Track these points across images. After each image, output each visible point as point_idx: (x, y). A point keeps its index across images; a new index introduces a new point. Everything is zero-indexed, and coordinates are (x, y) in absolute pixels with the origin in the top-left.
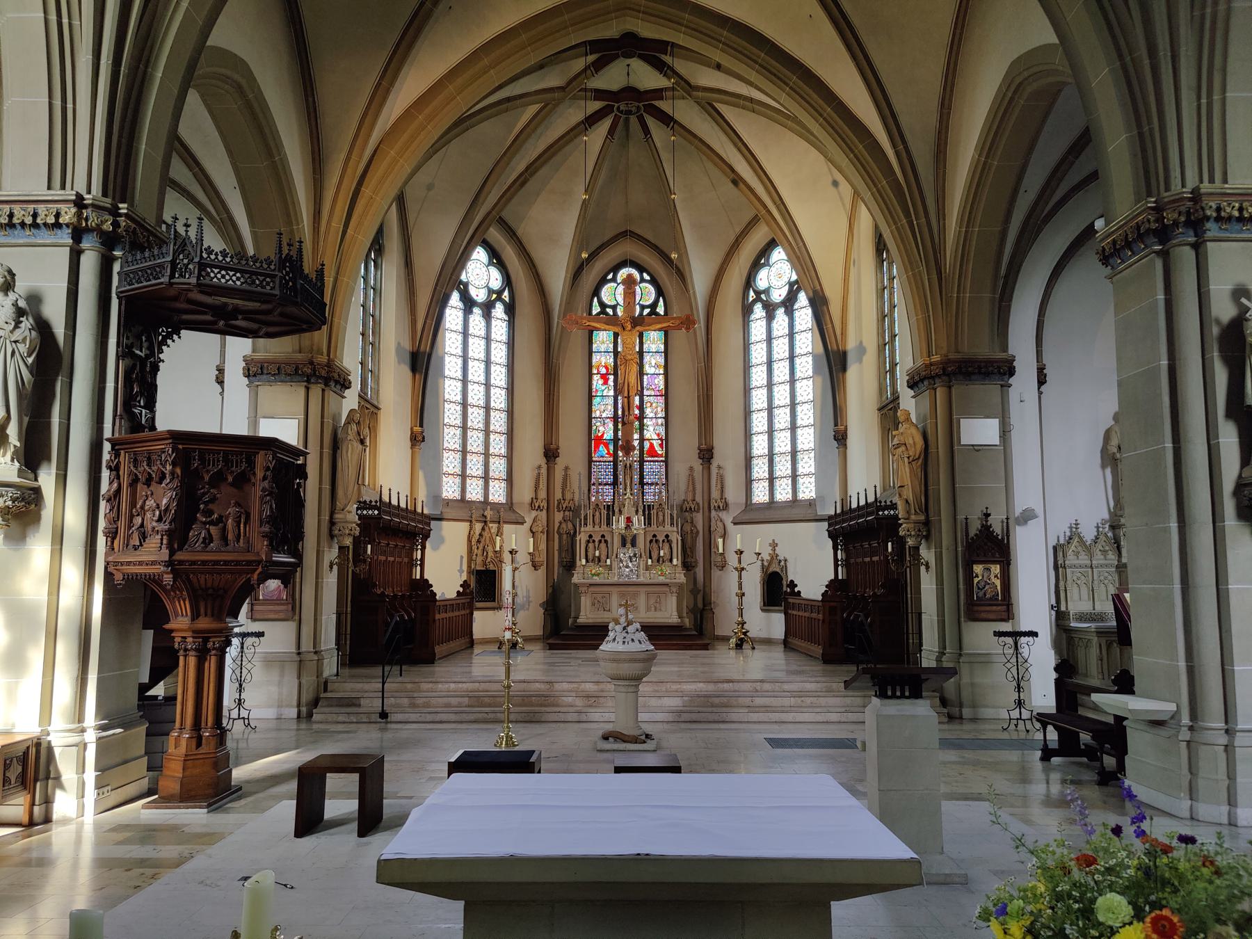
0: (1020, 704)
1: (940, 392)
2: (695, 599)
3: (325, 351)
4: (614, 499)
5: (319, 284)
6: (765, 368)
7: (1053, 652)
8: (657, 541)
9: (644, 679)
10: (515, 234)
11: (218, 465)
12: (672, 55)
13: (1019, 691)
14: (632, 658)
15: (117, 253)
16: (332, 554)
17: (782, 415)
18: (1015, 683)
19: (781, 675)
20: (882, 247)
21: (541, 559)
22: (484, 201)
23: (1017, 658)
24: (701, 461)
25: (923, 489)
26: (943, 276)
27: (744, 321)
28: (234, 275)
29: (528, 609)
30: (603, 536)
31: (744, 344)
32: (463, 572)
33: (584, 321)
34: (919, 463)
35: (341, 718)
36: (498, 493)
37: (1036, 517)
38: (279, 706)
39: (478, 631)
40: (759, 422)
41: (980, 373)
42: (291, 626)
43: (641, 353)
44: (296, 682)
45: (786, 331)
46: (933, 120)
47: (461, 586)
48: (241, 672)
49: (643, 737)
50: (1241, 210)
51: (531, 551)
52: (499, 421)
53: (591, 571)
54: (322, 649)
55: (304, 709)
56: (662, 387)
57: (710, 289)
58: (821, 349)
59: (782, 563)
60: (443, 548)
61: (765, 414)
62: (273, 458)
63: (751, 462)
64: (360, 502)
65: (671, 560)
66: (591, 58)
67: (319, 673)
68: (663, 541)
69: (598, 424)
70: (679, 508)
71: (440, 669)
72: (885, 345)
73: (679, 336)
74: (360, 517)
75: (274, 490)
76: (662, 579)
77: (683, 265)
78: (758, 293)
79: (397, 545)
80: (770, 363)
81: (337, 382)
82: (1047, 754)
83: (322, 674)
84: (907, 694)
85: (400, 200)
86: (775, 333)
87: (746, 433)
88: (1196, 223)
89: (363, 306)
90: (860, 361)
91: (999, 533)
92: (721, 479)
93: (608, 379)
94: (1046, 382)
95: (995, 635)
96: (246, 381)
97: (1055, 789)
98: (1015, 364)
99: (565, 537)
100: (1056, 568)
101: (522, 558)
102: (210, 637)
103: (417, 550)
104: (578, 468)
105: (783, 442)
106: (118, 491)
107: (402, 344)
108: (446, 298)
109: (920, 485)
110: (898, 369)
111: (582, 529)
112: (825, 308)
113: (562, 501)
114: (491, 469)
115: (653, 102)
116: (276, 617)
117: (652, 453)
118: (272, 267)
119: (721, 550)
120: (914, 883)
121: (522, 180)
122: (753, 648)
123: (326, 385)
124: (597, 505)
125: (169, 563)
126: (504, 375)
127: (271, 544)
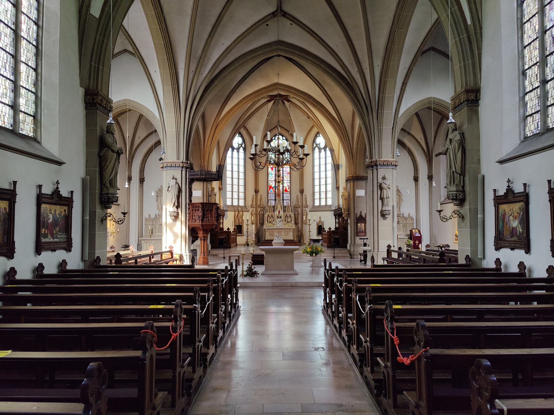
2: (298, 233)
30: (272, 215)
36: (242, 203)
40: (317, 182)
46: (351, 118)
50: (384, 163)
60: (227, 219)
65: (291, 222)
71: (232, 249)
76: (288, 227)
78: (316, 145)
88: (377, 166)
92: (306, 198)
101: (250, 222)
104: (265, 195)
105: (323, 188)
106: (190, 212)
117: (286, 190)
125: (202, 225)
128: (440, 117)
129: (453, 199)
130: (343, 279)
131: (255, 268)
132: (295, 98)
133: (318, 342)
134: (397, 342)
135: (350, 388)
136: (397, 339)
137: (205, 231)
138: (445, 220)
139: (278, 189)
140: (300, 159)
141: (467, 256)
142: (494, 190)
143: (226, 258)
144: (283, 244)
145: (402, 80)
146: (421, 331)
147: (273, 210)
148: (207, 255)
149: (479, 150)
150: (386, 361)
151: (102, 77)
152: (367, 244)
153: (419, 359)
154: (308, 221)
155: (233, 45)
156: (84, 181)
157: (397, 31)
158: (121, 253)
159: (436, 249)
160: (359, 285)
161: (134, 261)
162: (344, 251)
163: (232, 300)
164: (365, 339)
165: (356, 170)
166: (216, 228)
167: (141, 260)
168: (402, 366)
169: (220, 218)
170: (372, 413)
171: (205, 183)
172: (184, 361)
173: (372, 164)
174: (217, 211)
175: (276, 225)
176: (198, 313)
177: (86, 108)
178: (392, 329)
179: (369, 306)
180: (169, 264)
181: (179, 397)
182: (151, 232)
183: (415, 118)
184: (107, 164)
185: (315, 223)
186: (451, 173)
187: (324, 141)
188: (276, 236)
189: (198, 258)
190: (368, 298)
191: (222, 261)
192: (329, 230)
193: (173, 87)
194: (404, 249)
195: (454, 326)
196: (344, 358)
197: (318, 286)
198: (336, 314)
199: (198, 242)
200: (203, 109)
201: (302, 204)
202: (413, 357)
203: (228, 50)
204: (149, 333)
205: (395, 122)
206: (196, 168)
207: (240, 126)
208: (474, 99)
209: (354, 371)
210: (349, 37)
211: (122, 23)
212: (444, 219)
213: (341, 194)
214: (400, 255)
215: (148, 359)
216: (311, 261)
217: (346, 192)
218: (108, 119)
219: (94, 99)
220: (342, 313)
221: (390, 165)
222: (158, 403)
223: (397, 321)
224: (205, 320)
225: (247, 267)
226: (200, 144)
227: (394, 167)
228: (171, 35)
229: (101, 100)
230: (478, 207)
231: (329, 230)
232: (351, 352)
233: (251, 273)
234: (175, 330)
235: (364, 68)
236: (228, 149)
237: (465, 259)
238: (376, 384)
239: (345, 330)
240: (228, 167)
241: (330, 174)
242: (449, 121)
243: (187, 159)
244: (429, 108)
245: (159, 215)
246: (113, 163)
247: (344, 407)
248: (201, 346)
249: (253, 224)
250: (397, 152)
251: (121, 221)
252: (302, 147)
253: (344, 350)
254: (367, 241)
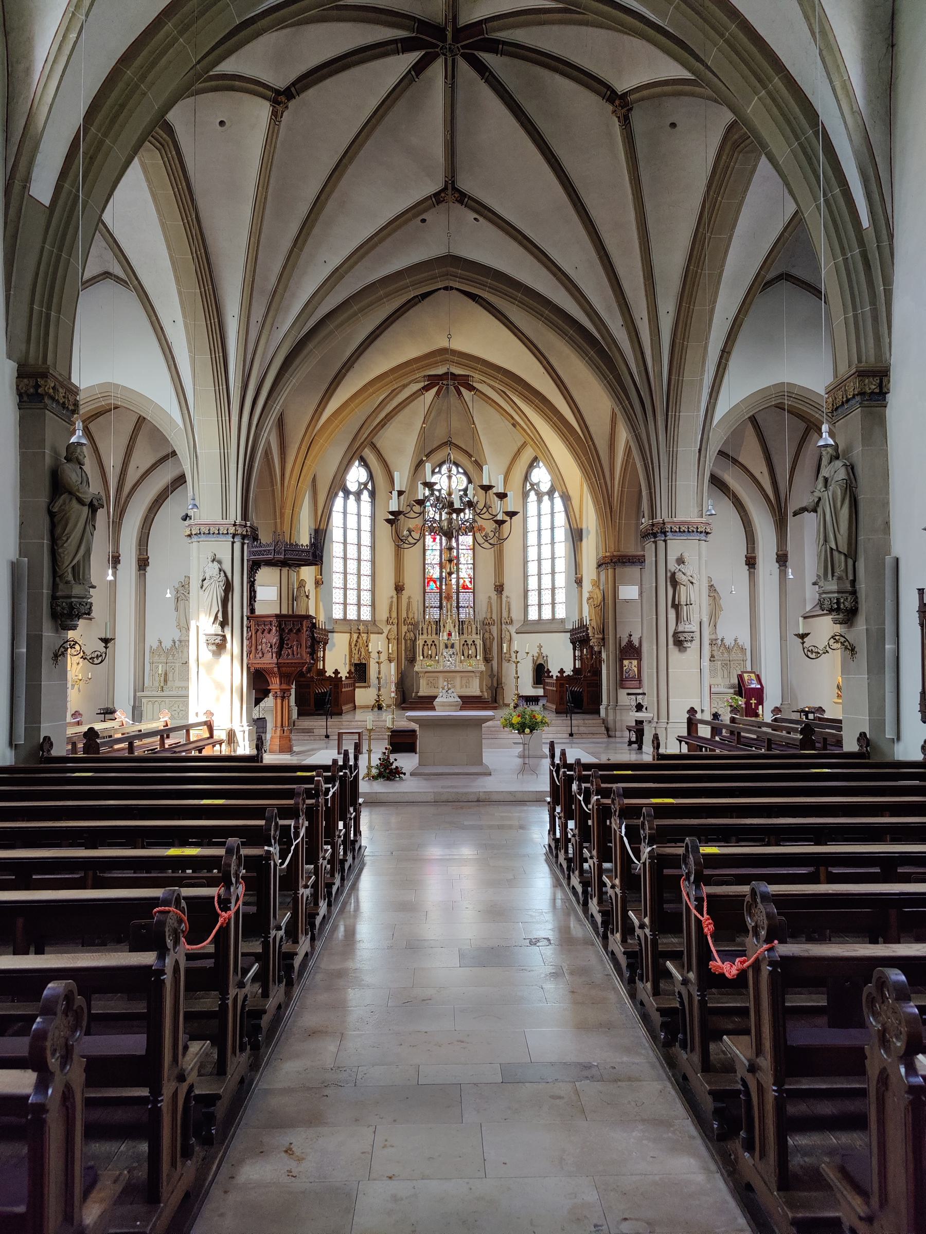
1: (610, 571)
15: (246, 541)
30: (433, 642)
36: (366, 615)
40: (532, 568)
50: (680, 528)
65: (476, 657)
71: (345, 717)
76: (470, 668)
78: (532, 485)
88: (665, 533)
92: (509, 604)
99: (409, 641)
101: (384, 657)
104: (417, 597)
105: (546, 582)
115: (476, 53)
125: (277, 664)
128: (803, 426)
129: (831, 609)
130: (593, 788)
131: (396, 760)
132: (485, 382)
133: (538, 926)
134: (708, 927)
135: (607, 1027)
136: (710, 921)
137: (285, 677)
138: (813, 656)
139: (446, 585)
140: (497, 522)
141: (863, 735)
142: (919, 590)
143: (331, 738)
144: (456, 706)
145: (720, 345)
146: (760, 906)
147: (436, 630)
148: (288, 729)
149: (888, 503)
150: (686, 968)
151: (56, 337)
152: (642, 706)
153: (756, 966)
154: (514, 655)
155: (346, 265)
156: (15, 568)
157: (710, 238)
158: (98, 726)
159: (795, 716)
160: (626, 801)
161: (124, 745)
162: (594, 721)
163: (347, 835)
164: (640, 920)
165: (618, 542)
166: (309, 670)
167: (141, 743)
168: (720, 980)
169: (318, 647)
170: (656, 1083)
171: (285, 570)
172: (245, 971)
173: (655, 529)
174: (312, 632)
176: (275, 865)
177: (21, 405)
178: (699, 900)
179: (649, 849)
180: (205, 753)
181: (234, 1053)
182: (162, 679)
183: (750, 430)
184: (66, 532)
185: (530, 659)
186: (826, 551)
187: (549, 478)
188: (443, 689)
189: (268, 736)
190: (647, 831)
191: (322, 744)
192: (559, 675)
193: (213, 356)
194: (726, 718)
195: (830, 892)
196: (594, 961)
197: (537, 799)
198: (574, 864)
199: (269, 702)
200: (279, 405)
201: (499, 616)
202: (744, 962)
203: (337, 276)
204: (171, 914)
205: (705, 437)
206: (265, 538)
207: (363, 443)
208: (877, 391)
209: (615, 989)
210: (604, 249)
211: (101, 216)
212: (813, 654)
213: (586, 595)
214: (715, 731)
215: (169, 969)
216: (520, 743)
217: (597, 590)
218: (73, 433)
219: (37, 386)
220: (590, 861)
221: (693, 531)
222: (190, 1067)
223: (709, 881)
224: (290, 881)
225: (380, 759)
226: (272, 483)
227: (703, 537)
228: (209, 241)
229: (54, 388)
230: (886, 627)
231: (559, 675)
232: (609, 949)
233: (387, 771)
234: (225, 904)
235: (636, 317)
236: (336, 495)
237: (858, 740)
238: (666, 1019)
239: (595, 900)
240: (336, 534)
241: (562, 549)
242: (821, 443)
243: (245, 516)
244: (780, 407)
245: (180, 641)
246: (83, 526)
247: (594, 1071)
248: (282, 938)
249: (390, 661)
250: (709, 506)
251: (97, 657)
252: (502, 496)
253: (593, 944)
254: (643, 700)
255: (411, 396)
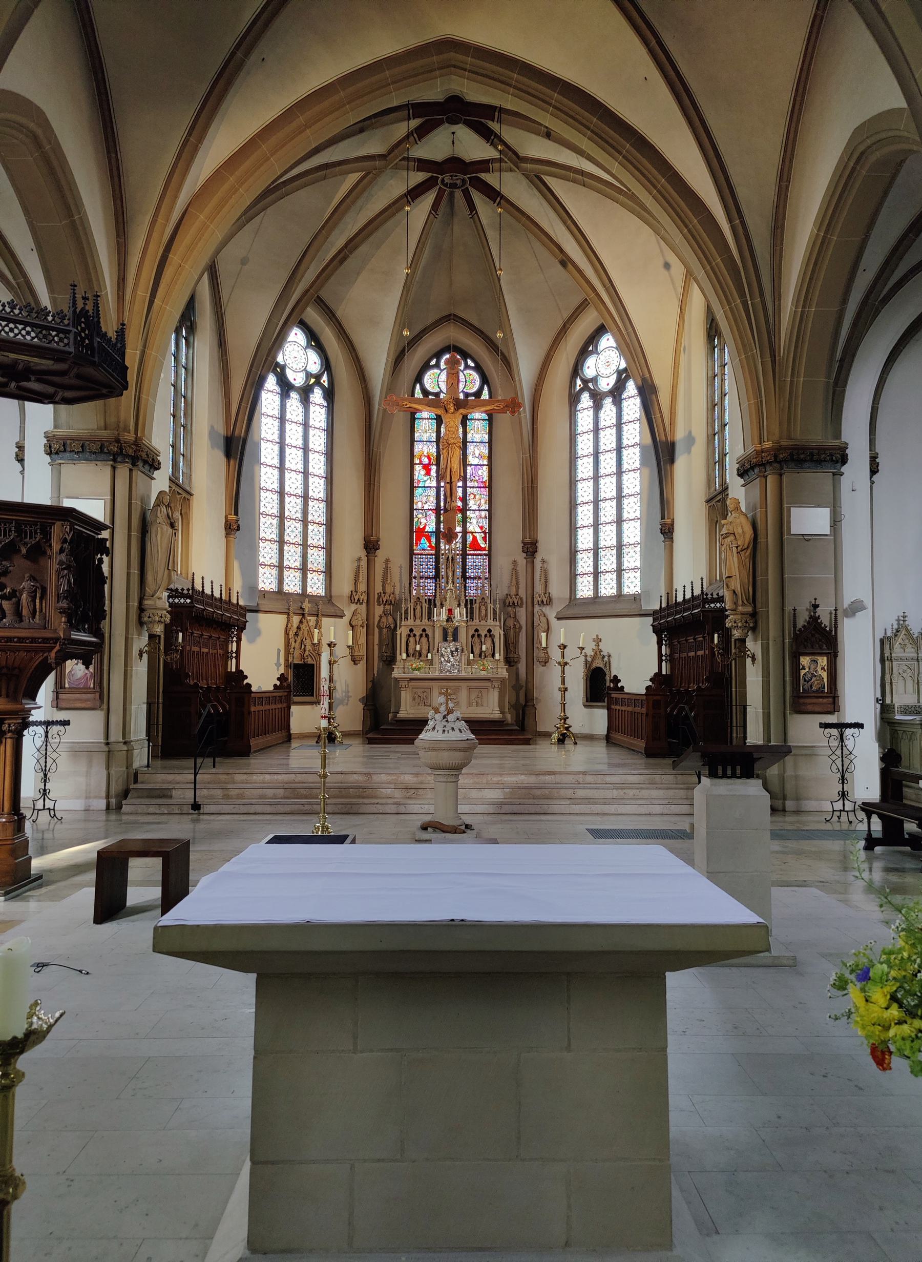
0: (843, 795)
3: (132, 428)
4: (435, 593)
5: (119, 345)
6: (591, 460)
7: (877, 744)
8: (479, 636)
9: (463, 771)
10: (334, 315)
11: (10, 536)
12: (500, 121)
13: (843, 783)
14: (452, 747)
16: (141, 642)
17: (609, 508)
18: (839, 775)
19: (604, 768)
20: (713, 333)
21: (360, 654)
22: (302, 276)
23: (842, 749)
24: (525, 555)
25: (751, 580)
26: (777, 358)
27: (570, 411)
28: (24, 329)
29: (347, 704)
30: (424, 630)
31: (571, 435)
32: (280, 665)
33: (406, 403)
34: (748, 554)
35: (152, 809)
36: (316, 585)
37: (863, 608)
38: (87, 798)
39: (296, 726)
40: (584, 515)
41: (812, 460)
42: (98, 716)
43: (465, 442)
44: (105, 773)
45: (614, 421)
46: (771, 192)
47: (278, 679)
48: (46, 762)
49: (463, 827)
51: (350, 644)
52: (317, 512)
53: (412, 665)
54: (132, 739)
55: (113, 801)
56: (486, 478)
57: (537, 376)
58: (648, 440)
59: (606, 659)
60: (259, 640)
61: (591, 507)
62: (71, 530)
63: (575, 556)
64: (171, 590)
65: (493, 655)
66: (414, 123)
67: (129, 765)
68: (486, 636)
69: (420, 516)
70: (502, 604)
71: (256, 762)
72: (715, 435)
73: (504, 420)
74: (171, 605)
75: (72, 564)
76: (484, 674)
77: (509, 352)
78: (585, 382)
79: (211, 637)
80: (596, 454)
81: (145, 462)
82: (871, 843)
83: (132, 764)
84: (738, 771)
85: (212, 270)
86: (602, 424)
87: (571, 526)
89: (174, 386)
90: (689, 451)
91: (828, 624)
92: (545, 573)
93: (431, 469)
94: (878, 471)
95: (820, 727)
96: (47, 458)
97: (878, 876)
98: (848, 451)
99: (385, 631)
100: (882, 661)
101: (341, 651)
102: (5, 719)
103: (232, 642)
104: (399, 560)
107: (215, 427)
108: (261, 381)
109: (748, 576)
110: (727, 459)
111: (403, 623)
112: (654, 397)
113: (383, 595)
114: (309, 560)
115: (479, 175)
116: (83, 705)
117: (475, 545)
118: (66, 322)
119: (544, 645)
120: (761, 950)
121: (342, 256)
122: (576, 743)
123: (134, 464)
124: (418, 598)
126: (323, 463)
127: (69, 621)
175: (437, 666)
201: (529, 592)
255: (390, 206)
